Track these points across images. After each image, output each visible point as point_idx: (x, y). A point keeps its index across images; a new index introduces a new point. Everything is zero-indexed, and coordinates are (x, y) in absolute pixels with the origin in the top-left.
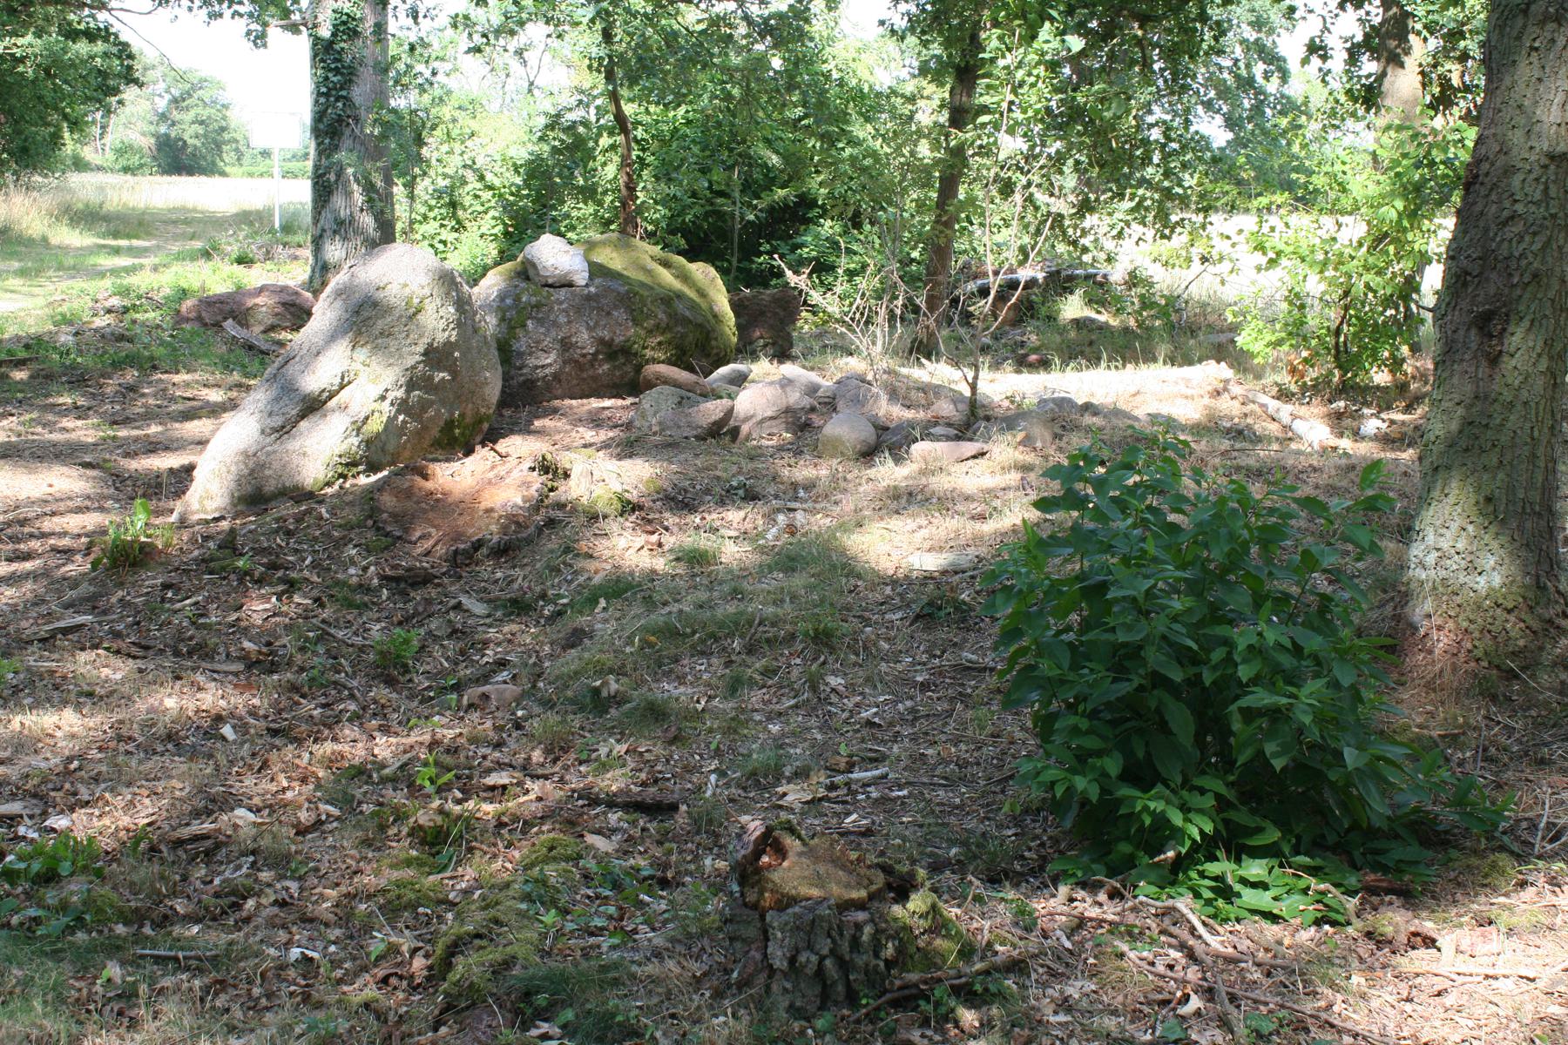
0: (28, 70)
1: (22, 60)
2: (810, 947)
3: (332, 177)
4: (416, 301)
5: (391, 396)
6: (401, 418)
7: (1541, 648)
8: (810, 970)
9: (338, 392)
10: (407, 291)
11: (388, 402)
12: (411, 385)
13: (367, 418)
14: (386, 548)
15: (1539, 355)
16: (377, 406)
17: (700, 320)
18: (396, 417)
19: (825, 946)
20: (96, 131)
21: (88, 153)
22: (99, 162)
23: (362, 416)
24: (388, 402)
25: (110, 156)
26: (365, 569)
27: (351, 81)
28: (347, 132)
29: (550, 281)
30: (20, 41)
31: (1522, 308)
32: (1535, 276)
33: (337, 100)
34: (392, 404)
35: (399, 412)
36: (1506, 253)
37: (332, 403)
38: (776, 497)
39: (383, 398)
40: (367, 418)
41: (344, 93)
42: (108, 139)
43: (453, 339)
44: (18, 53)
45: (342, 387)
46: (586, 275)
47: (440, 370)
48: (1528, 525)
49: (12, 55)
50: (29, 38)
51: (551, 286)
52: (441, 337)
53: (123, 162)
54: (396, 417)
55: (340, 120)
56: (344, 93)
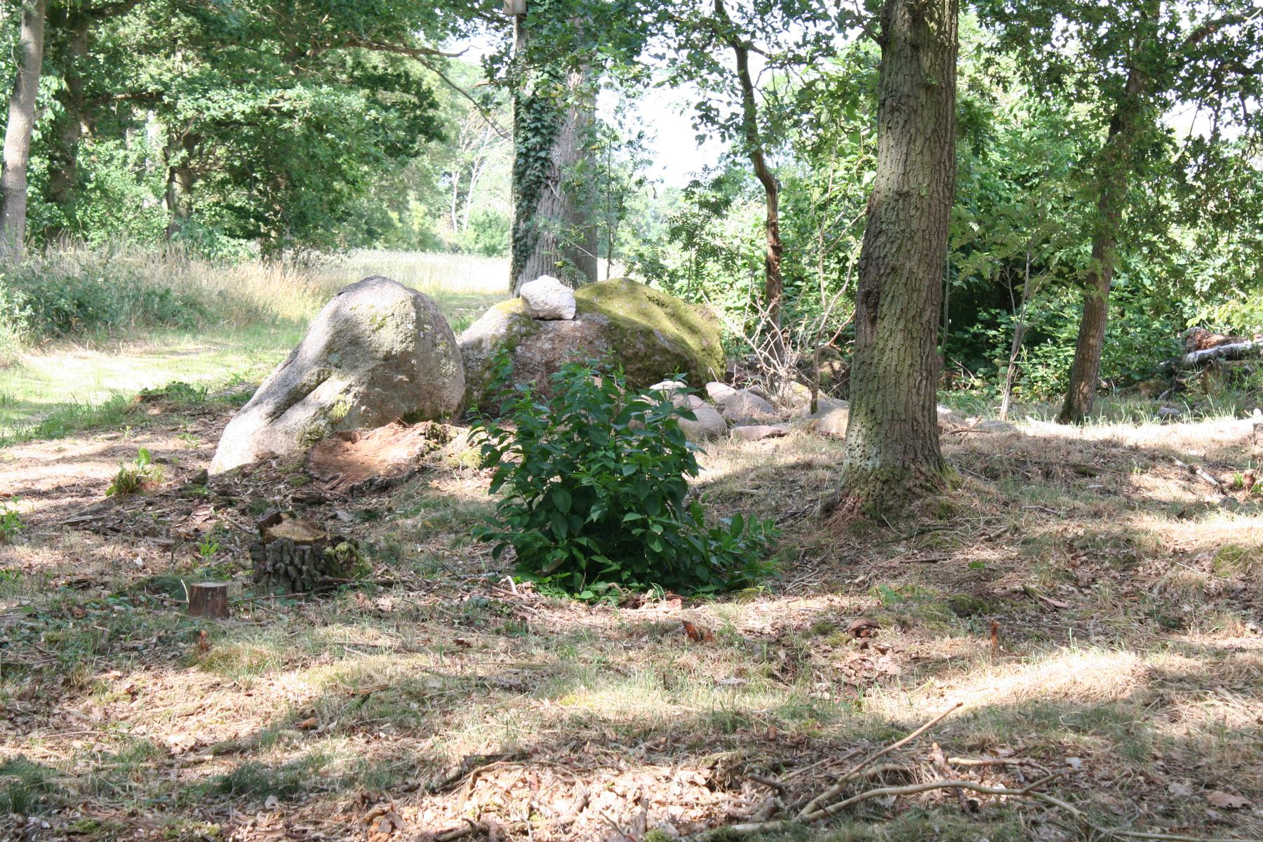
0: (297, 126)
1: (290, 114)
2: (282, 561)
3: (530, 242)
4: (379, 319)
5: (355, 390)
6: (363, 408)
7: (902, 506)
8: (282, 571)
9: (315, 387)
10: (373, 311)
11: (351, 395)
12: (372, 383)
13: (333, 406)
14: (305, 484)
15: (899, 319)
16: (342, 397)
17: (678, 351)
18: (358, 407)
19: (287, 559)
20: (452, 199)
21: (442, 230)
22: (454, 240)
23: (328, 404)
24: (351, 395)
25: (470, 233)
26: (286, 496)
27: (551, 141)
28: (546, 193)
29: (541, 315)
30: (289, 93)
31: (886, 289)
32: (893, 269)
33: (536, 161)
34: (355, 396)
35: (361, 403)
36: (876, 254)
37: (311, 396)
38: (761, 512)
39: (347, 391)
40: (333, 406)
41: (542, 154)
42: (467, 209)
43: (410, 349)
44: (286, 106)
45: (319, 383)
46: (573, 310)
47: (399, 373)
48: (897, 427)
49: (278, 109)
50: (299, 89)
51: (542, 319)
52: (398, 348)
53: (485, 240)
54: (358, 407)
55: (538, 182)
56: (542, 154)
